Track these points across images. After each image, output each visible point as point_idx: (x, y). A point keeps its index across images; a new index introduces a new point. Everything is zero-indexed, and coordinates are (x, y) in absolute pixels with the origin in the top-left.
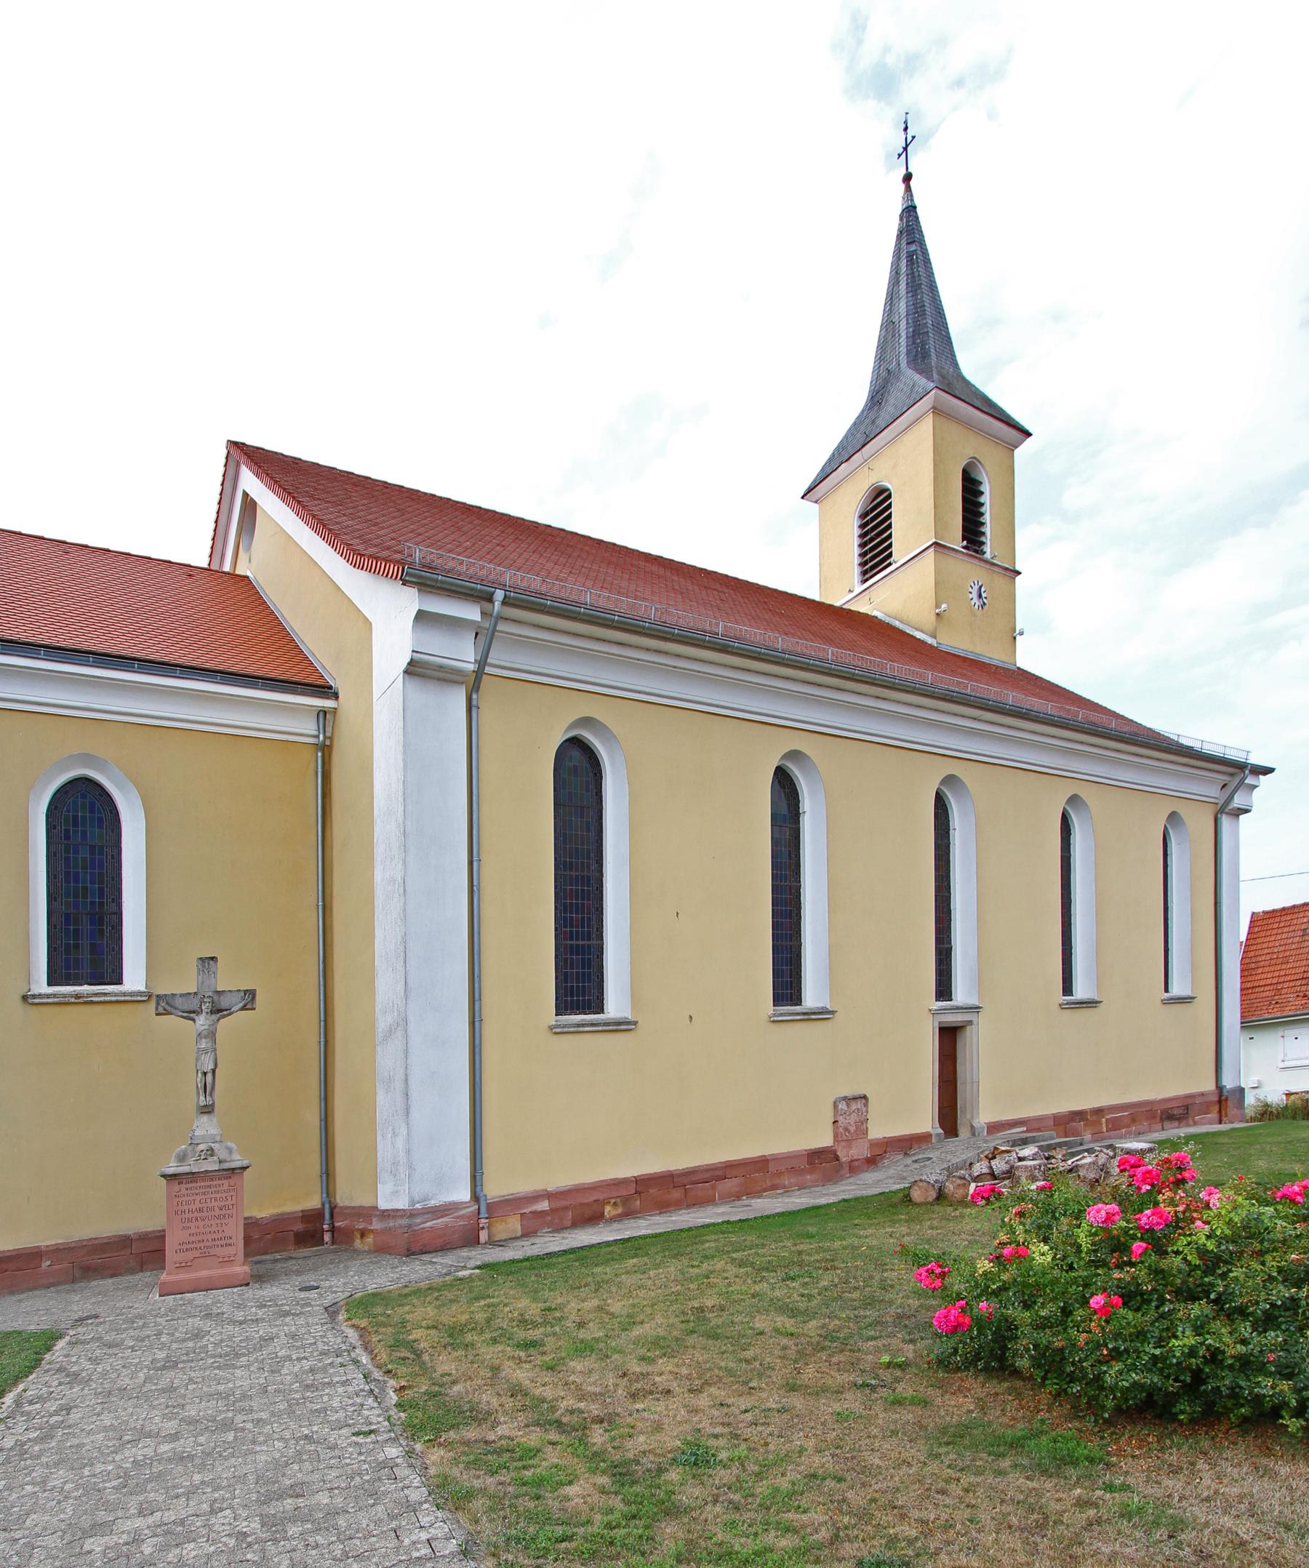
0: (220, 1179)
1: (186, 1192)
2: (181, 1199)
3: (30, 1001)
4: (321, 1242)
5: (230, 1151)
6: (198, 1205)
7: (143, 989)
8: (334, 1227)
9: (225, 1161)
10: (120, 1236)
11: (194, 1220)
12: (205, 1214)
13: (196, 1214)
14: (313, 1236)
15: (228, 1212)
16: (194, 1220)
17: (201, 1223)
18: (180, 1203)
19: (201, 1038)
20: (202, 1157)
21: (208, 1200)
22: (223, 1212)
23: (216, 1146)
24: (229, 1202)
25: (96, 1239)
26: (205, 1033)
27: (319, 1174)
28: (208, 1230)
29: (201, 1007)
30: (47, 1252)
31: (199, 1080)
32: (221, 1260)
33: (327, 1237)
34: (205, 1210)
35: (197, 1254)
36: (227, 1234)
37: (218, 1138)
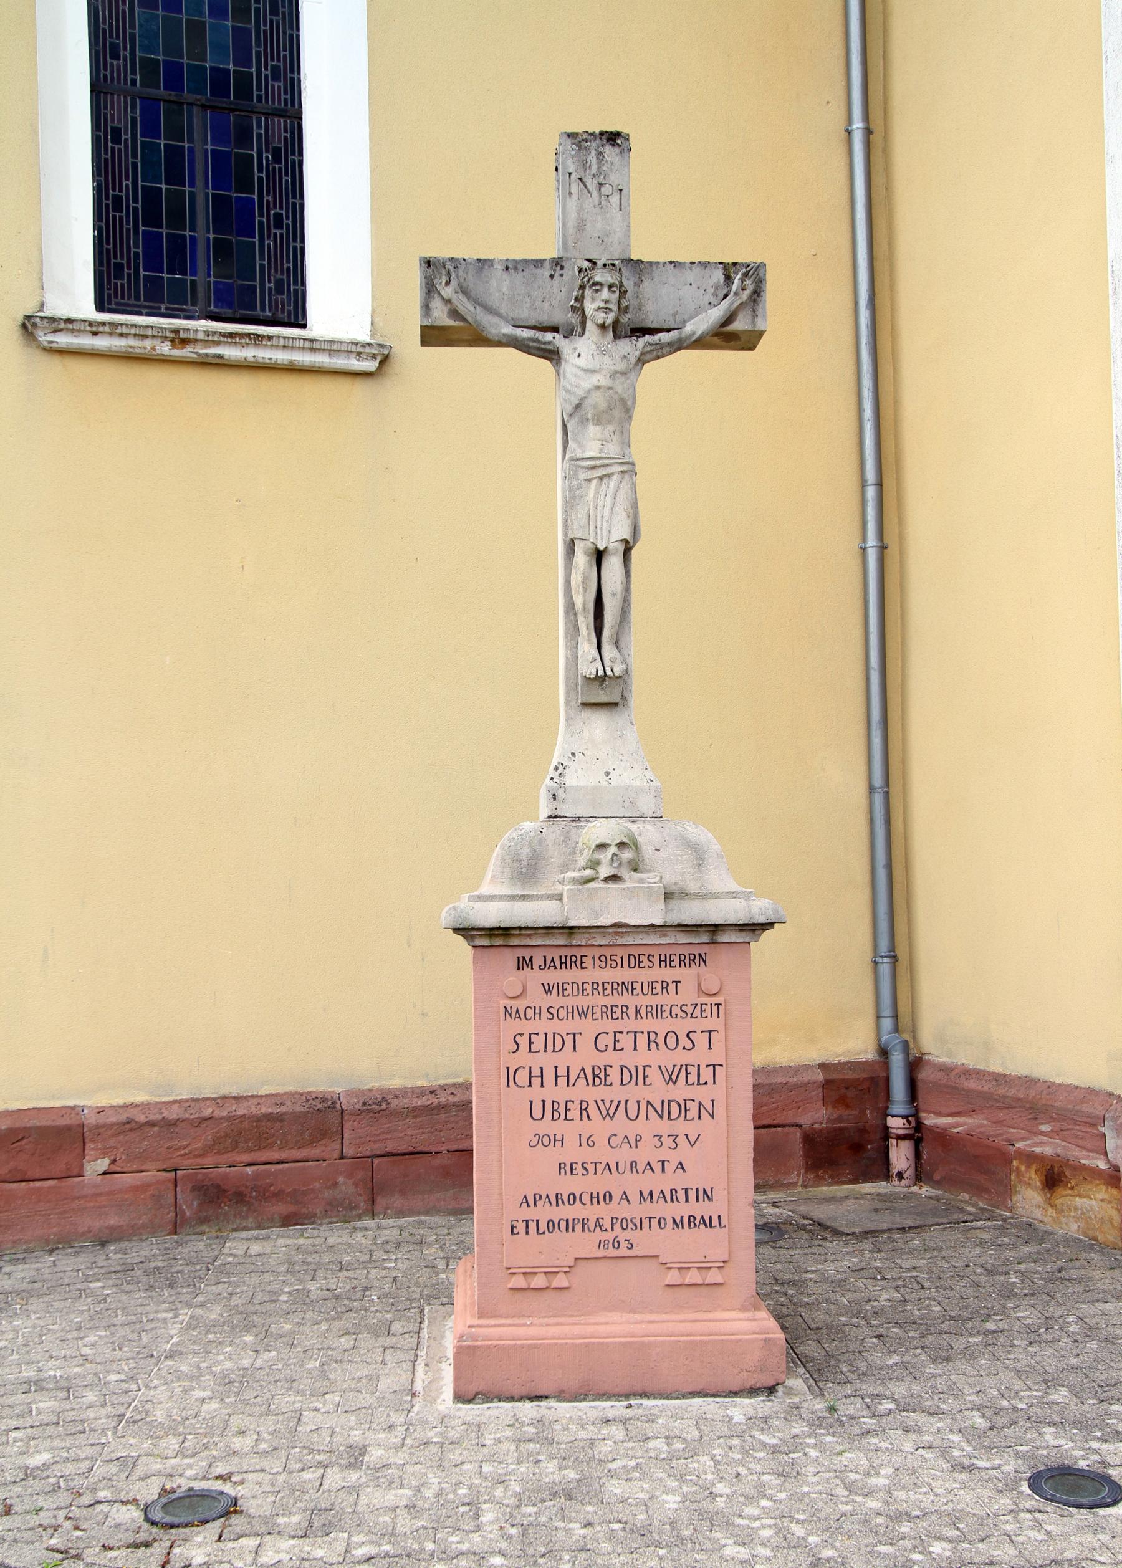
0: (666, 961)
1: (544, 1001)
2: (527, 1027)
3: (44, 338)
4: (882, 1169)
5: (699, 858)
6: (586, 1057)
7: (364, 336)
8: (919, 1126)
9: (684, 895)
10: (308, 1097)
11: (574, 1113)
12: (616, 1093)
13: (581, 1091)
14: (857, 1148)
15: (702, 1094)
16: (574, 1113)
17: (598, 1127)
18: (523, 1042)
19: (584, 421)
20: (604, 871)
21: (626, 1041)
22: (680, 1091)
23: (646, 834)
24: (700, 1056)
25: (237, 1098)
26: (598, 400)
27: (868, 956)
28: (625, 1155)
29: (579, 309)
30: (99, 1130)
31: (576, 578)
32: (673, 1277)
33: (900, 1156)
34: (614, 1075)
35: (584, 1243)
36: (694, 1179)
37: (647, 805)
